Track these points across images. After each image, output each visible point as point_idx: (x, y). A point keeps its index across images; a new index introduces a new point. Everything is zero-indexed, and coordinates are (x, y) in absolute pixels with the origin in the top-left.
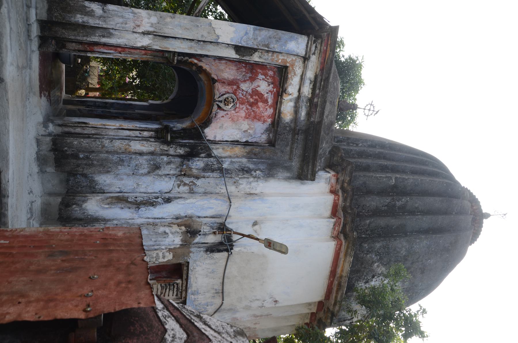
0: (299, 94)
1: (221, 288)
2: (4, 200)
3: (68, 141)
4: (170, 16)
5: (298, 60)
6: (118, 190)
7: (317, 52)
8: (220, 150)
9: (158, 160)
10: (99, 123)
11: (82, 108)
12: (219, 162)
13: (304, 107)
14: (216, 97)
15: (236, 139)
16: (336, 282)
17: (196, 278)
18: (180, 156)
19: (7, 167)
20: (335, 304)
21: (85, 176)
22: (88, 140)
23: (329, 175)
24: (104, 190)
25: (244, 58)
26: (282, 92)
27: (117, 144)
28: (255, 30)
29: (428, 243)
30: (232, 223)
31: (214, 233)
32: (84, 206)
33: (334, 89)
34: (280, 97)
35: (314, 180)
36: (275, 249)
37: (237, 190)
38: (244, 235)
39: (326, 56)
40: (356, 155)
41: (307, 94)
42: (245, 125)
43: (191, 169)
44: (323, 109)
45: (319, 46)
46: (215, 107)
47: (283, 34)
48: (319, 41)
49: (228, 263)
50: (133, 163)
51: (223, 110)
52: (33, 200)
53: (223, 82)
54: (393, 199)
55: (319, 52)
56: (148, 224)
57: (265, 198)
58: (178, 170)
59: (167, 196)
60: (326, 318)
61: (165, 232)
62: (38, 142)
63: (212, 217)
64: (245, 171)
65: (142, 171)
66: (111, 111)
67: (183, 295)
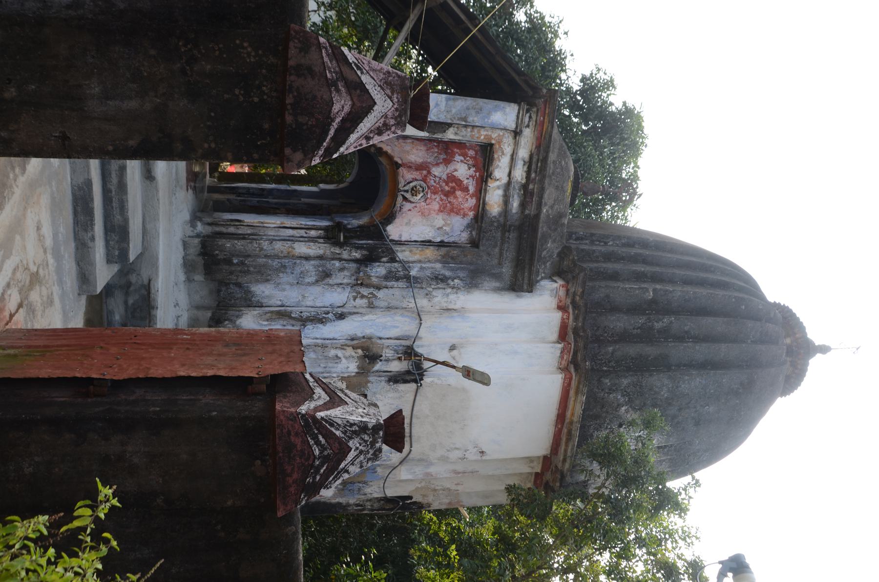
2: (153, 312)
3: (220, 243)
6: (279, 303)
7: (532, 124)
8: (407, 253)
9: (328, 266)
10: (256, 221)
11: (232, 197)
12: (405, 269)
13: (516, 196)
15: (428, 238)
16: (565, 430)
18: (356, 261)
19: (157, 275)
20: (564, 460)
21: (239, 285)
22: (242, 242)
23: (555, 285)
24: (262, 303)
25: (436, 136)
28: (447, 100)
29: (704, 382)
30: (422, 346)
31: (400, 359)
32: (238, 322)
33: (562, 169)
35: (531, 292)
36: (474, 380)
37: (430, 304)
38: (437, 362)
40: (601, 259)
41: (519, 179)
43: (369, 277)
44: (541, 197)
46: (400, 199)
48: (535, 109)
49: (417, 398)
50: (298, 270)
51: (411, 202)
53: (409, 166)
54: (649, 319)
56: (316, 345)
57: (466, 315)
58: (353, 278)
59: (340, 311)
60: (554, 481)
61: (337, 356)
62: (185, 245)
63: (397, 339)
64: (440, 280)
65: (308, 280)
66: (271, 200)
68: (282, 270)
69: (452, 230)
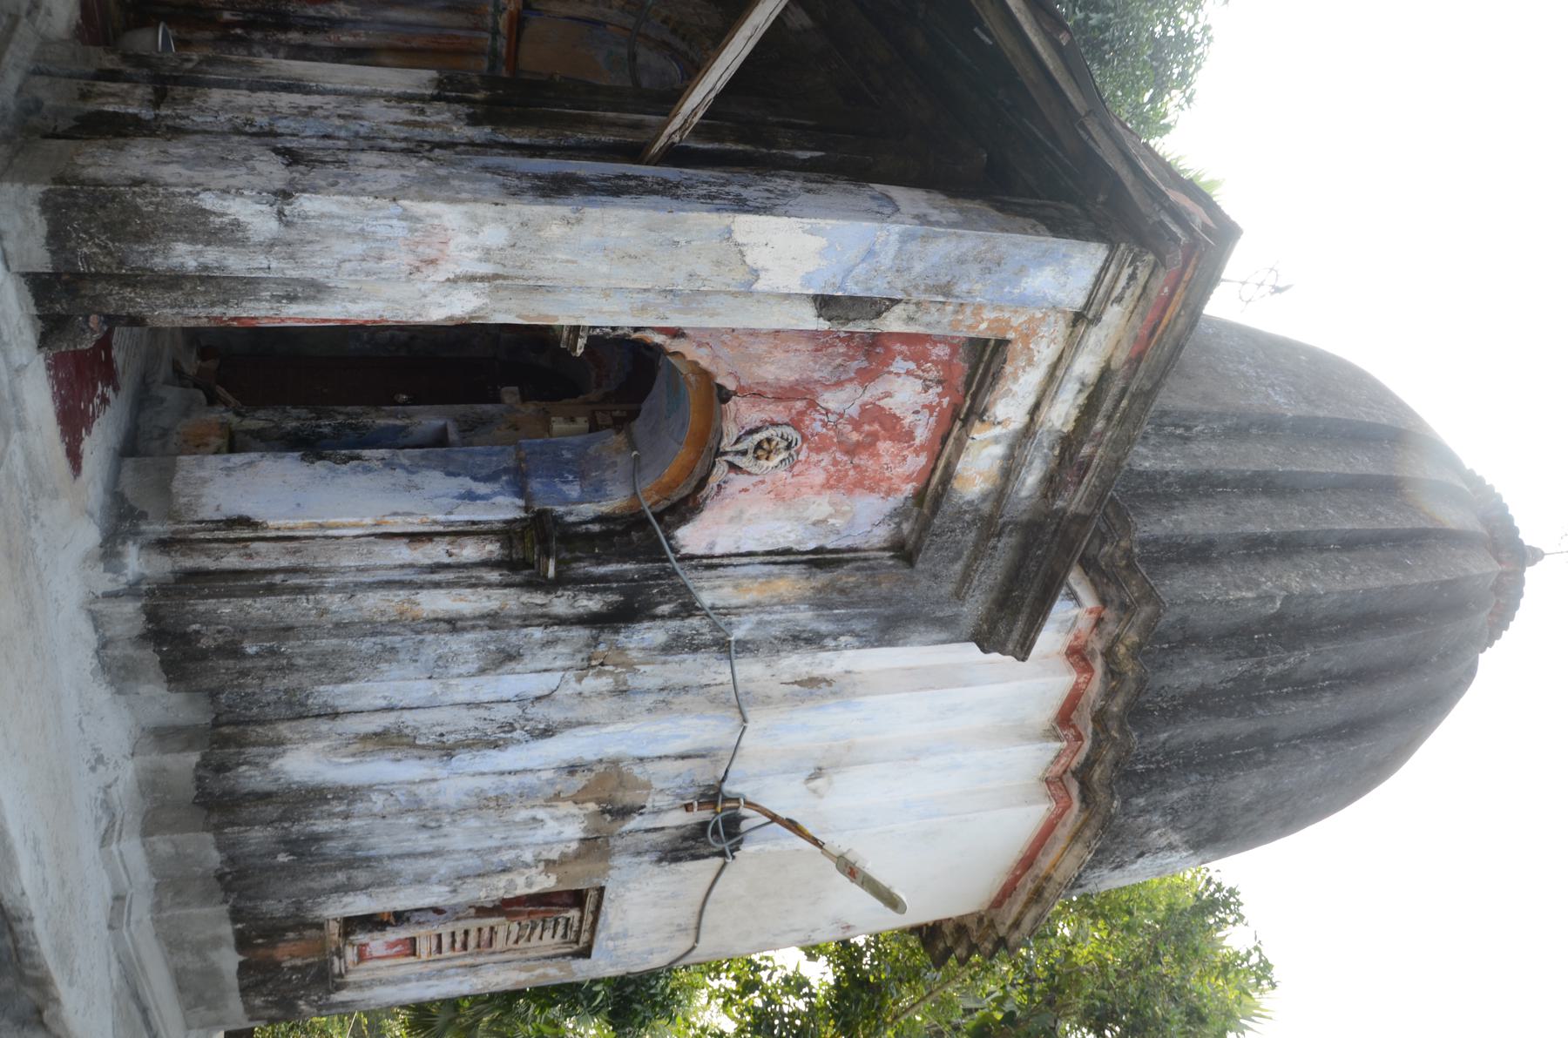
0: (1032, 419)
1: (694, 921)
3: (201, 608)
4: (563, 218)
5: (1052, 319)
12: (715, 627)
14: (725, 441)
15: (783, 544)
17: (624, 912)
26: (971, 411)
27: (374, 603)
34: (958, 424)
35: (1024, 660)
38: (774, 818)
39: (1161, 319)
42: (821, 507)
45: (1142, 276)
47: (1015, 245)
52: (110, 781)
55: (1138, 292)
67: (584, 937)
68: (386, 655)
69: (851, 524)
